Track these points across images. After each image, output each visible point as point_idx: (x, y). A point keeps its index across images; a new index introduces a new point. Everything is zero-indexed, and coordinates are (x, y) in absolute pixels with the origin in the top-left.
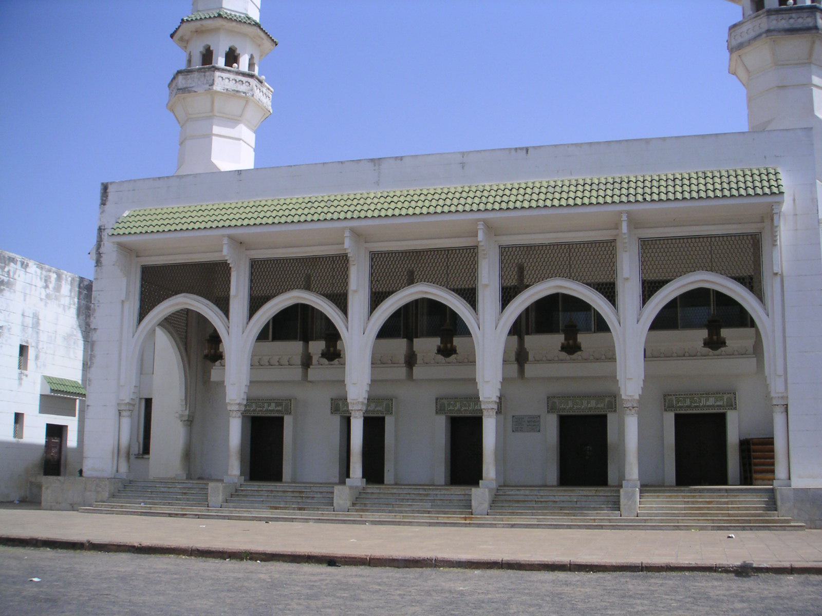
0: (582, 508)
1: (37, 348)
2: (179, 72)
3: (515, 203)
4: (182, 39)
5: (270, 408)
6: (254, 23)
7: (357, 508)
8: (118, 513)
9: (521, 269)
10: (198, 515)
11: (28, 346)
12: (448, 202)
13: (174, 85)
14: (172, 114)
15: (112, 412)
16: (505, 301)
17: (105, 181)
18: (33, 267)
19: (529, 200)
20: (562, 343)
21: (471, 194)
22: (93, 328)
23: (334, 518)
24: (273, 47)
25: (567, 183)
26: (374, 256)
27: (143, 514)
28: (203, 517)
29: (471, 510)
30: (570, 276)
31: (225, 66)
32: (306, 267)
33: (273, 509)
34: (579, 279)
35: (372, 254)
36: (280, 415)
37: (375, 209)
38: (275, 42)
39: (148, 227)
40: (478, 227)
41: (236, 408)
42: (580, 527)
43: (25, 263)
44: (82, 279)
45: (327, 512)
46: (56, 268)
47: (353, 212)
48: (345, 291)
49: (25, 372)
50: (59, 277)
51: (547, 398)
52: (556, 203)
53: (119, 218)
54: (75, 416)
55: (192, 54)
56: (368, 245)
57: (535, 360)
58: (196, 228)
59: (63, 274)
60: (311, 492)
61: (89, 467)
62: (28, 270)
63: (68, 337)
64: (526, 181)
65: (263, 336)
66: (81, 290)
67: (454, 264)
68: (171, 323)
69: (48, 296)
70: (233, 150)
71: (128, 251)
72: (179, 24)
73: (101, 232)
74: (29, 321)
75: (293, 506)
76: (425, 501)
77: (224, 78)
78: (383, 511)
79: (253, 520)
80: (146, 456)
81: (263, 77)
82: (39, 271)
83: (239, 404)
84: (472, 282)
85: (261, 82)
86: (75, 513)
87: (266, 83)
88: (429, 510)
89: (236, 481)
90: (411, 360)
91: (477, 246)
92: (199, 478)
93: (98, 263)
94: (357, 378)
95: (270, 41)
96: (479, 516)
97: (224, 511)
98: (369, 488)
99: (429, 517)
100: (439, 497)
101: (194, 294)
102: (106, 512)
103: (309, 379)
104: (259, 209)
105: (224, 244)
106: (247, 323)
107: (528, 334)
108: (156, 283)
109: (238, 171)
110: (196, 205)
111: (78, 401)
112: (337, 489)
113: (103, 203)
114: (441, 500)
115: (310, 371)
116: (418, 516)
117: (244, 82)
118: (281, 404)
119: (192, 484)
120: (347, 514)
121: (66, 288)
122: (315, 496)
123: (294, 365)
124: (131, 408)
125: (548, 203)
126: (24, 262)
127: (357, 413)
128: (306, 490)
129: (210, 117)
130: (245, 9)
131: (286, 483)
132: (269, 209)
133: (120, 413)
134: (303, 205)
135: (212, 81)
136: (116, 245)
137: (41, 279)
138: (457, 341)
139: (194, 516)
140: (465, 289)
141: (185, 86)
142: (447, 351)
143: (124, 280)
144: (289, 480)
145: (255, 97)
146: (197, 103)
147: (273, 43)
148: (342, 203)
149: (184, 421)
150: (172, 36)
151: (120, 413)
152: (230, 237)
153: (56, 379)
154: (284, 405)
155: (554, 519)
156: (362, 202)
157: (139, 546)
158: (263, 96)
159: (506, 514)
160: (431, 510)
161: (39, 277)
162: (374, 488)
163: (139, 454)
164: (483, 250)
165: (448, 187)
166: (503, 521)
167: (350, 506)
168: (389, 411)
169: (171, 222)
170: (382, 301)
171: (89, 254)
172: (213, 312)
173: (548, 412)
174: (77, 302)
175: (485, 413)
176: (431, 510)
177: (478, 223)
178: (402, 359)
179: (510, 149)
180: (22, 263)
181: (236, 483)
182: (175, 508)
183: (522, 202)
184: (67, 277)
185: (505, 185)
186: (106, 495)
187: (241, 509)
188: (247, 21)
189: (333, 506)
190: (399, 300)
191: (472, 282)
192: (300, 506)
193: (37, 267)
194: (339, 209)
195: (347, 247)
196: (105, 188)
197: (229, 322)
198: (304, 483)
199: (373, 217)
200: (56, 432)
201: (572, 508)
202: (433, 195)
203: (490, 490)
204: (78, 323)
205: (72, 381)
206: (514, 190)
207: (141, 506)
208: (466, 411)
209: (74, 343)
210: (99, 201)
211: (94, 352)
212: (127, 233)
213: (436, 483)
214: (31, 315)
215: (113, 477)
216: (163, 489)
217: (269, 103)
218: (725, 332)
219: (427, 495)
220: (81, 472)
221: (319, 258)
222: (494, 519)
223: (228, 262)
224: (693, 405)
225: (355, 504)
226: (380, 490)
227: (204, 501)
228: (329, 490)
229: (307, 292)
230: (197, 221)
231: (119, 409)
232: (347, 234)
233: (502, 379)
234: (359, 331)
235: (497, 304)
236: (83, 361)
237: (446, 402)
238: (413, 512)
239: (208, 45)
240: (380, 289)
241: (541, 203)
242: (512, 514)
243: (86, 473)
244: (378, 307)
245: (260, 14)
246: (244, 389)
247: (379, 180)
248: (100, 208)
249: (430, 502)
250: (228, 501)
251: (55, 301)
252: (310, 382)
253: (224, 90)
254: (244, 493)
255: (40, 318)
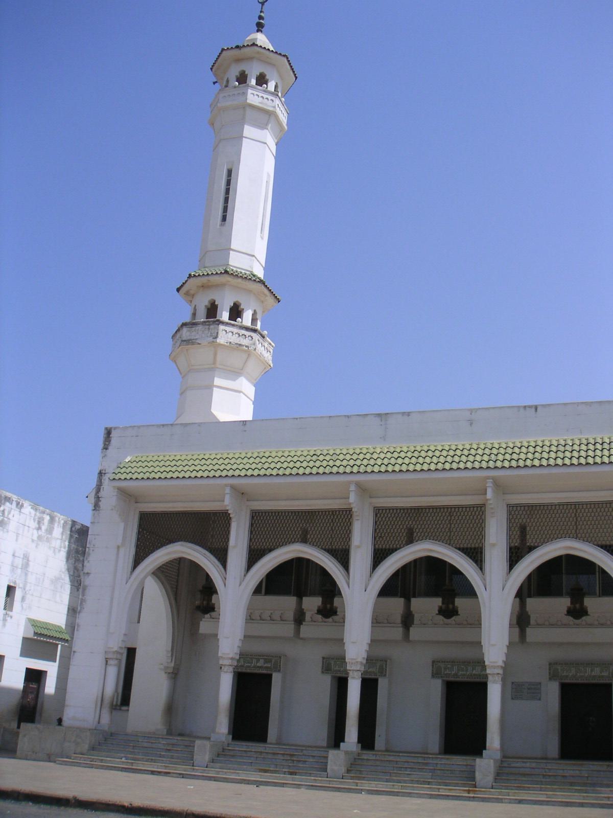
0: (594, 785)
1: (25, 589)
2: (184, 325)
3: (525, 461)
4: (187, 293)
5: (258, 665)
6: (258, 280)
7: (352, 775)
8: (98, 767)
9: (523, 530)
10: (183, 774)
11: (15, 587)
12: (456, 459)
13: (178, 335)
14: (174, 365)
15: (99, 660)
16: (512, 561)
17: (109, 426)
18: (28, 508)
19: (539, 458)
20: (568, 607)
21: (480, 452)
22: (86, 572)
23: (328, 785)
24: (275, 304)
25: (578, 442)
26: (379, 511)
27: (124, 769)
28: (187, 776)
29: (192, 762)
30: (448, 541)
31: (229, 320)
32: (301, 521)
33: (261, 772)
34: (589, 540)
35: (376, 509)
36: (269, 672)
37: (382, 464)
38: (278, 299)
39: (150, 473)
40: (487, 485)
41: (227, 662)
42: (593, 805)
43: (21, 504)
44: (74, 523)
45: (320, 779)
46: (49, 510)
47: (359, 466)
48: (347, 547)
49: (10, 613)
50: (52, 520)
51: (549, 665)
52: (567, 461)
53: (120, 463)
54: (55, 662)
55: (197, 307)
56: (374, 500)
57: (538, 624)
58: (199, 476)
59: (56, 516)
60: (303, 755)
61: (70, 715)
62: (23, 510)
63: (55, 581)
64: (535, 439)
65: (257, 591)
66: (72, 534)
67: (328, 526)
68: (163, 572)
69: (40, 538)
70: (233, 402)
71: (127, 496)
72: (186, 279)
73: (102, 475)
74: (19, 562)
75: (284, 770)
76: (424, 770)
77: (228, 331)
78: (379, 780)
79: (241, 783)
80: (124, 708)
81: (265, 333)
82: (33, 512)
83: (232, 659)
84: (479, 541)
85: (264, 337)
86: (52, 764)
87: (267, 338)
88: (429, 780)
89: (223, 739)
90: (407, 620)
91: (485, 505)
92: (180, 735)
93: (96, 506)
94: (357, 638)
95: (273, 298)
96: (483, 790)
97: (211, 772)
98: (363, 753)
99: (430, 788)
100: (439, 767)
101: (192, 543)
102: (85, 765)
103: (302, 635)
104: (263, 460)
105: (352, 491)
106: (245, 576)
107: (530, 596)
108: (153, 529)
109: (243, 421)
110: (198, 453)
111: (59, 646)
112: (332, 754)
113: (106, 448)
114: (442, 770)
115: (303, 628)
116: (417, 787)
117: (247, 336)
118: (270, 661)
119: (174, 740)
120: (341, 782)
121: (58, 531)
122: (307, 760)
123: (285, 621)
124: (119, 657)
125: (559, 462)
126: (19, 503)
127: (356, 673)
128: (297, 753)
129: (212, 369)
130: (251, 267)
131: (271, 744)
132: (274, 460)
133: (107, 662)
134: (309, 458)
135: (216, 334)
136: (116, 490)
137: (34, 520)
138: (459, 602)
139: (178, 775)
140: (471, 549)
141: (188, 338)
142: (448, 612)
143: (122, 525)
144: (274, 741)
145: (257, 351)
146: (200, 355)
147: (275, 300)
148: (348, 457)
149: (169, 673)
150: (178, 290)
151: (107, 662)
152: (233, 487)
153: (40, 622)
154: (273, 662)
155: (564, 795)
156: (368, 456)
157: (130, 806)
158: (265, 350)
159: (513, 788)
160: (431, 780)
161: (32, 518)
162: (368, 755)
163: (116, 705)
164: (492, 508)
165: (456, 444)
166: (509, 796)
167: (345, 773)
168: (383, 672)
169: (173, 469)
170: (385, 558)
171: (87, 497)
172: (210, 562)
173: (550, 679)
174: (67, 546)
175: (490, 678)
176: (431, 780)
177: (488, 480)
178: (399, 619)
179: (519, 407)
180: (18, 504)
181: (224, 742)
182: (158, 765)
183: (532, 460)
184: (60, 519)
185: (514, 443)
186: (87, 746)
187: (229, 771)
188: (252, 278)
189: (192, 760)
190: (402, 558)
191: (479, 541)
192: (291, 771)
193: (32, 508)
194: (345, 463)
195: (227, 504)
196: (108, 432)
197: (226, 574)
198: (288, 745)
199: (458, 468)
200: (34, 677)
201: (585, 784)
202: (399, 453)
203: (495, 761)
204: (66, 567)
205: (55, 626)
206: (465, 450)
207: (122, 762)
208: (464, 675)
209: (61, 587)
210: (101, 445)
211: (85, 596)
212: (128, 478)
213: (429, 752)
214: (22, 556)
215: (94, 728)
216: (146, 745)
217: (270, 358)
218: (588, 602)
219: (427, 764)
220: (60, 721)
221: (319, 512)
222: (500, 793)
223: (229, 512)
224: (578, 674)
225: (351, 770)
226: (376, 756)
227: (189, 759)
228: (323, 754)
229: (304, 545)
230: (200, 470)
231: (107, 657)
232: (353, 488)
233: (370, 640)
234: (360, 589)
235: (505, 565)
236: (69, 605)
237: (442, 665)
238: (412, 781)
239: (213, 299)
240: (391, 546)
241: (552, 462)
242: (519, 788)
243: (66, 721)
244: (382, 564)
245: (264, 272)
246: (238, 643)
247: (385, 435)
248: (102, 452)
249: (430, 772)
250: (214, 761)
251: (46, 543)
252: (302, 639)
253: (227, 343)
254: (231, 753)
255: (30, 559)
